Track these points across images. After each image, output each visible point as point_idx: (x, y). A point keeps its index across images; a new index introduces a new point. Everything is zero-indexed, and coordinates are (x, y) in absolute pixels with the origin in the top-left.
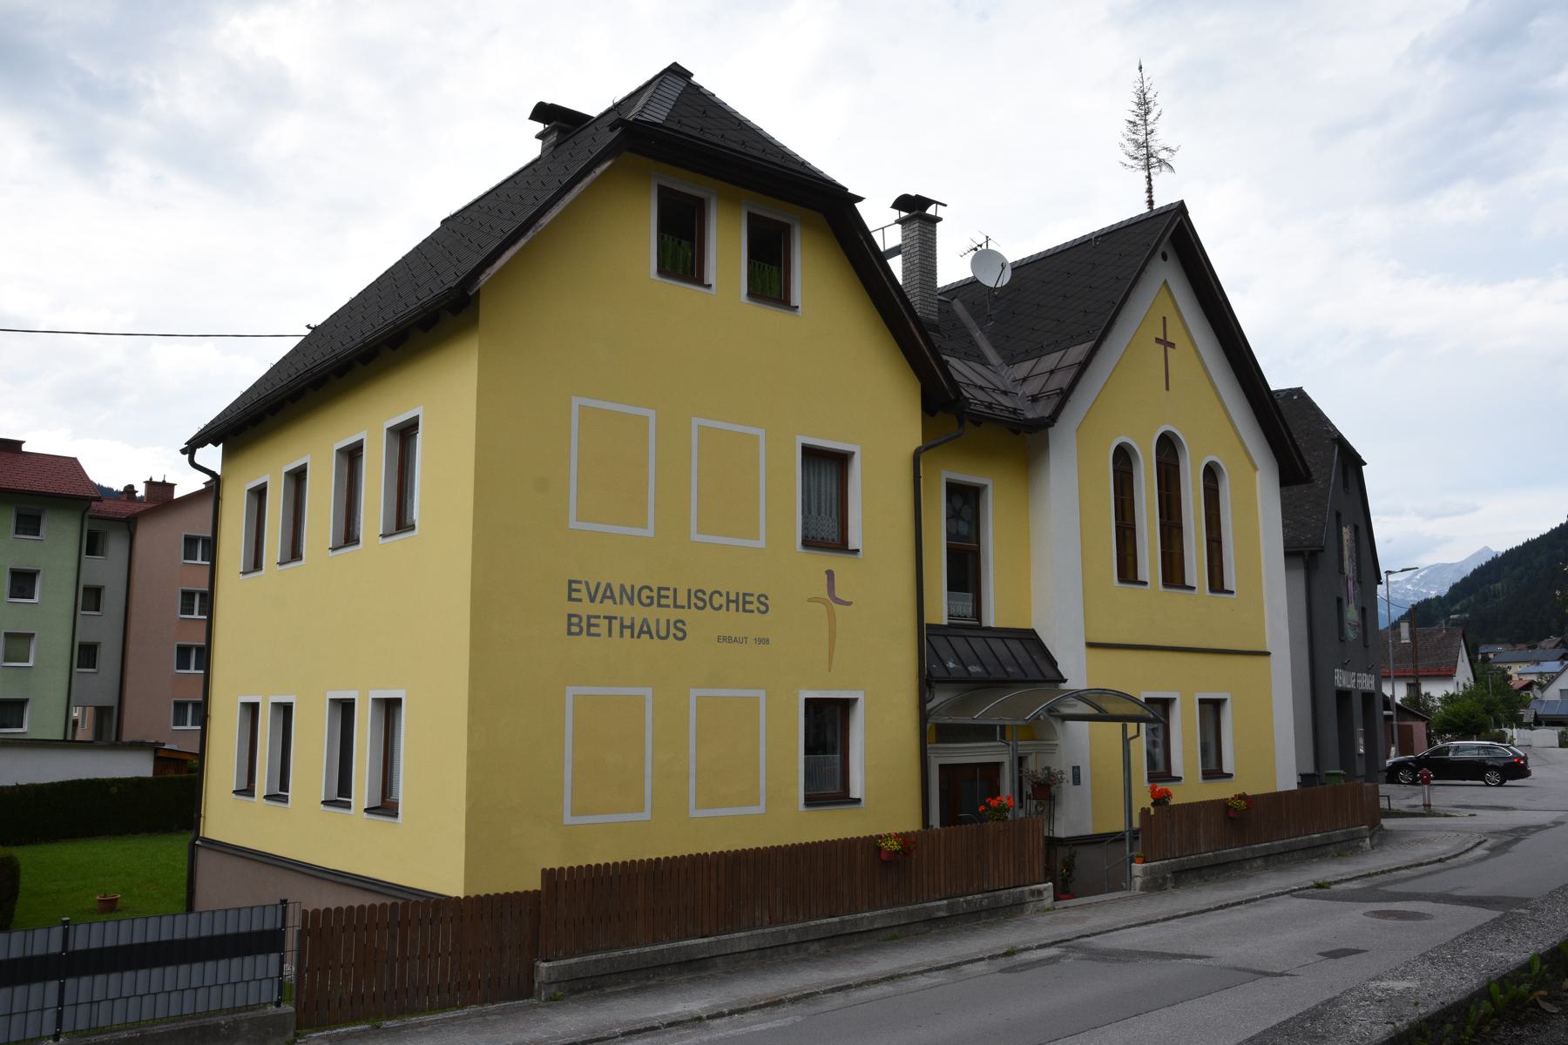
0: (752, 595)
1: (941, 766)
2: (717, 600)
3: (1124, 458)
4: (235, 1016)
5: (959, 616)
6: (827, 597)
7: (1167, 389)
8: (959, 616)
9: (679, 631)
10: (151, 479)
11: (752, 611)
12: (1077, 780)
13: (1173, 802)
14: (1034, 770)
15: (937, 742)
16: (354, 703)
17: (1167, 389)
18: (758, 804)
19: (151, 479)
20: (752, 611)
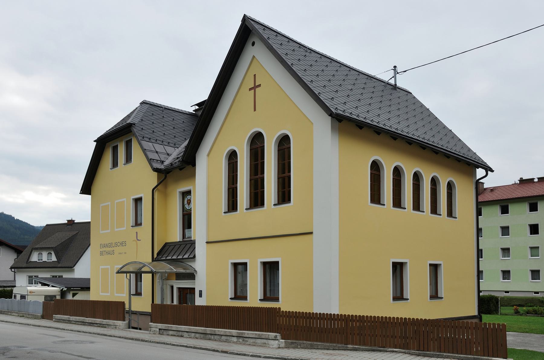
0: (123, 242)
1: (179, 289)
2: (119, 244)
3: (232, 156)
4: (4, 288)
5: (189, 237)
6: (136, 240)
7: (255, 110)
8: (189, 237)
9: (113, 253)
10: (72, 219)
11: (123, 246)
12: (201, 296)
13: (199, 302)
14: (513, 311)
15: (176, 280)
16: (482, 229)
17: (255, 110)
18: (124, 294)
19: (72, 219)
20: (123, 246)
